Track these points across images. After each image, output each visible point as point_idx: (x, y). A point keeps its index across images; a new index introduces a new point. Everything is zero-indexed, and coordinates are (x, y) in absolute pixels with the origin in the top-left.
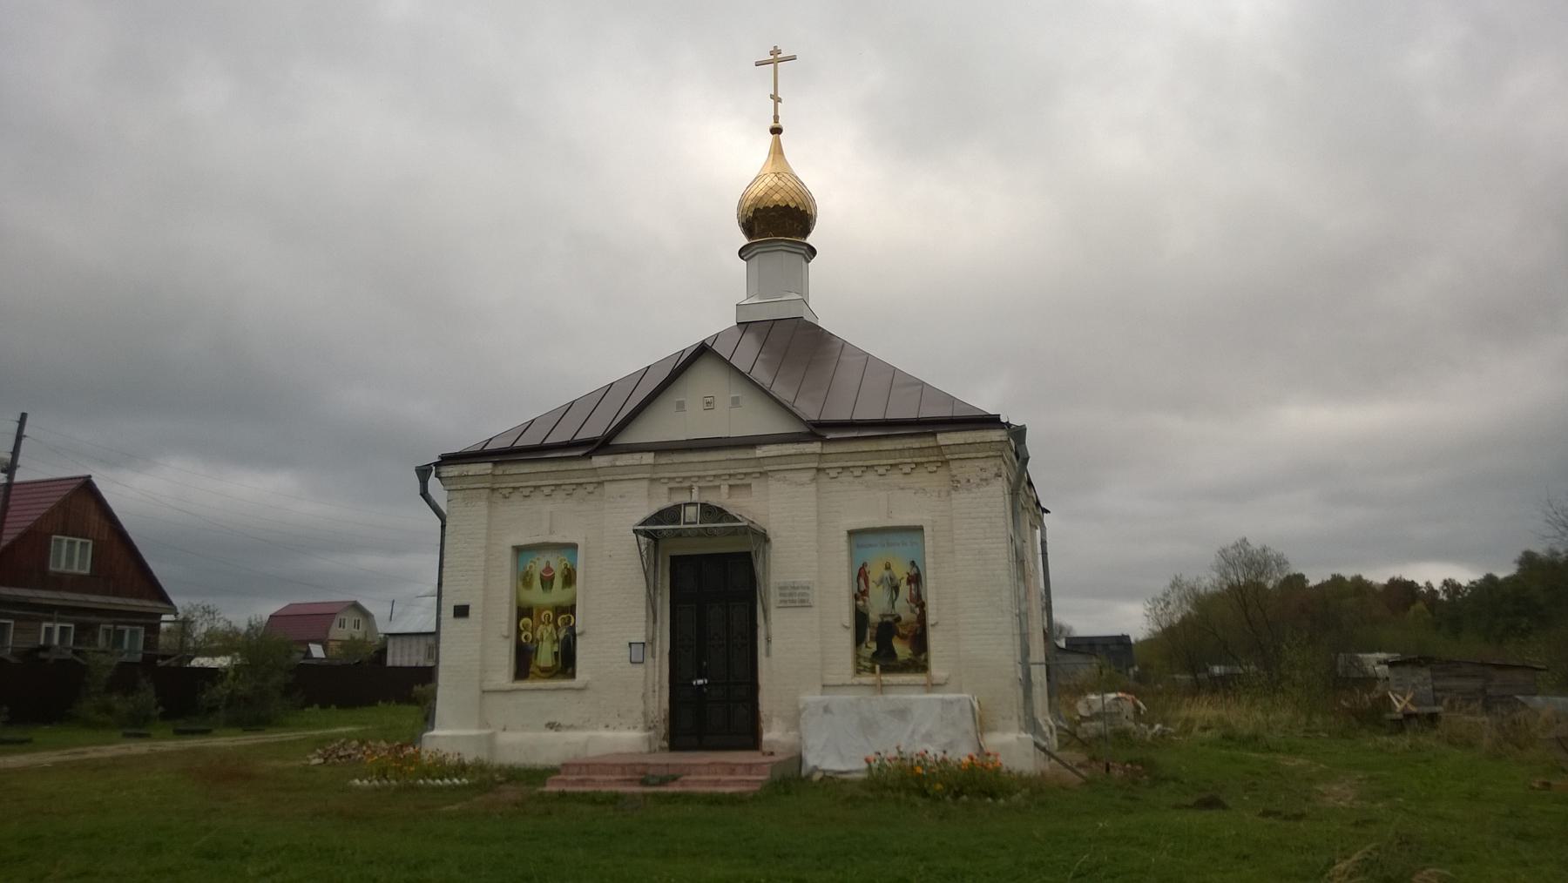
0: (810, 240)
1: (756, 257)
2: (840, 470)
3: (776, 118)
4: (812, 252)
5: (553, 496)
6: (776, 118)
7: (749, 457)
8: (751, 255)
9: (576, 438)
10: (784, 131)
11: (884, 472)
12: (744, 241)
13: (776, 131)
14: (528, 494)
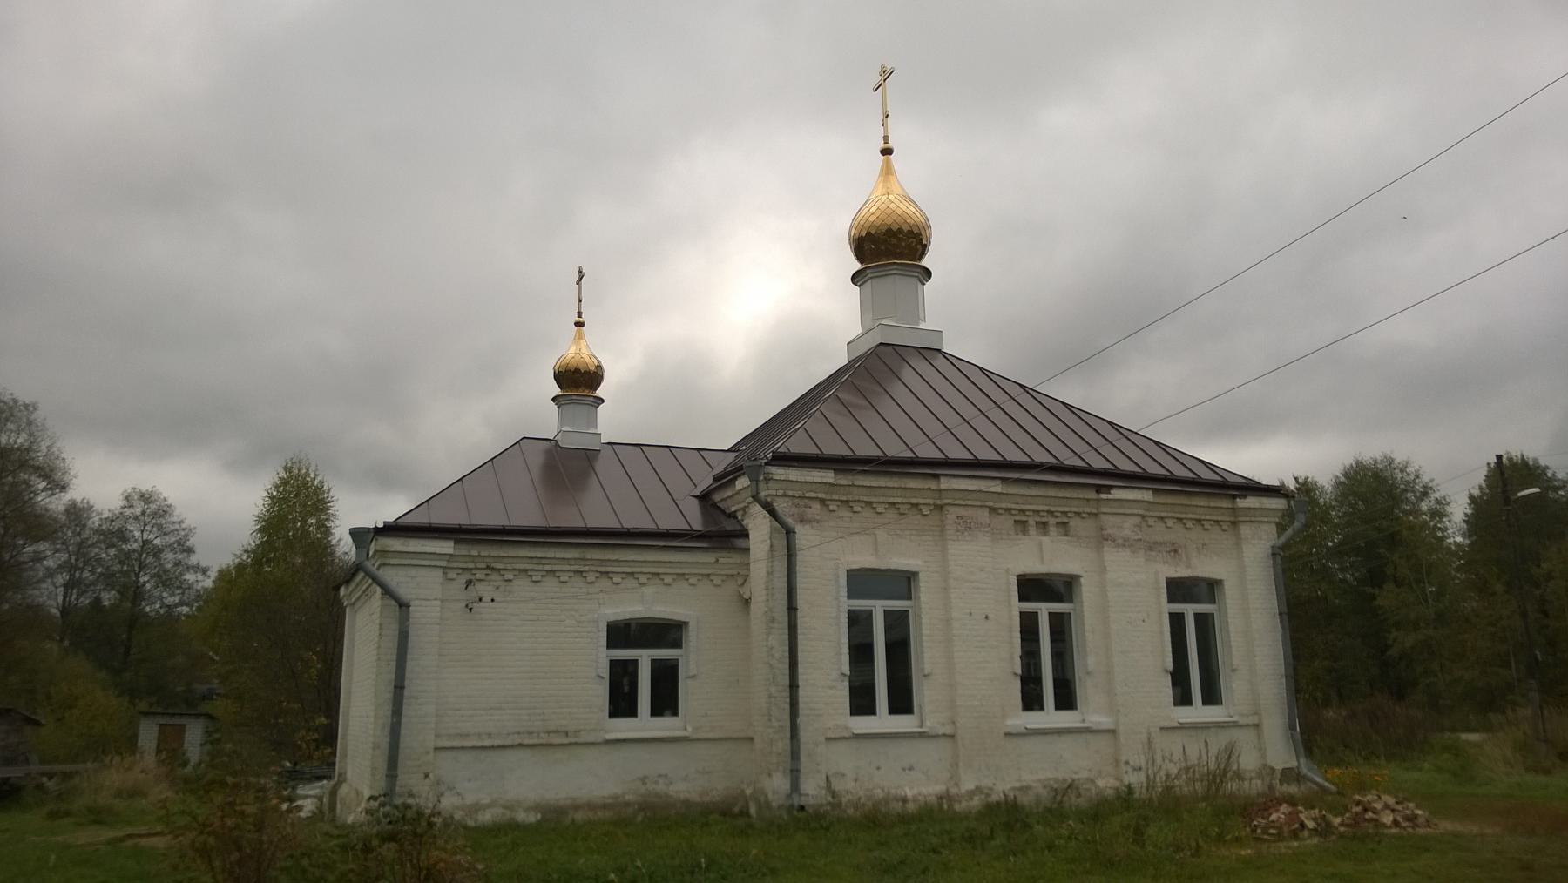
0: (925, 262)
1: (870, 282)
2: (460, 571)
3: (886, 139)
4: (927, 273)
5: (622, 586)
6: (886, 139)
7: (607, 558)
8: (876, 274)
10: (880, 155)
11: (539, 578)
12: (857, 266)
13: (887, 152)
14: (694, 583)
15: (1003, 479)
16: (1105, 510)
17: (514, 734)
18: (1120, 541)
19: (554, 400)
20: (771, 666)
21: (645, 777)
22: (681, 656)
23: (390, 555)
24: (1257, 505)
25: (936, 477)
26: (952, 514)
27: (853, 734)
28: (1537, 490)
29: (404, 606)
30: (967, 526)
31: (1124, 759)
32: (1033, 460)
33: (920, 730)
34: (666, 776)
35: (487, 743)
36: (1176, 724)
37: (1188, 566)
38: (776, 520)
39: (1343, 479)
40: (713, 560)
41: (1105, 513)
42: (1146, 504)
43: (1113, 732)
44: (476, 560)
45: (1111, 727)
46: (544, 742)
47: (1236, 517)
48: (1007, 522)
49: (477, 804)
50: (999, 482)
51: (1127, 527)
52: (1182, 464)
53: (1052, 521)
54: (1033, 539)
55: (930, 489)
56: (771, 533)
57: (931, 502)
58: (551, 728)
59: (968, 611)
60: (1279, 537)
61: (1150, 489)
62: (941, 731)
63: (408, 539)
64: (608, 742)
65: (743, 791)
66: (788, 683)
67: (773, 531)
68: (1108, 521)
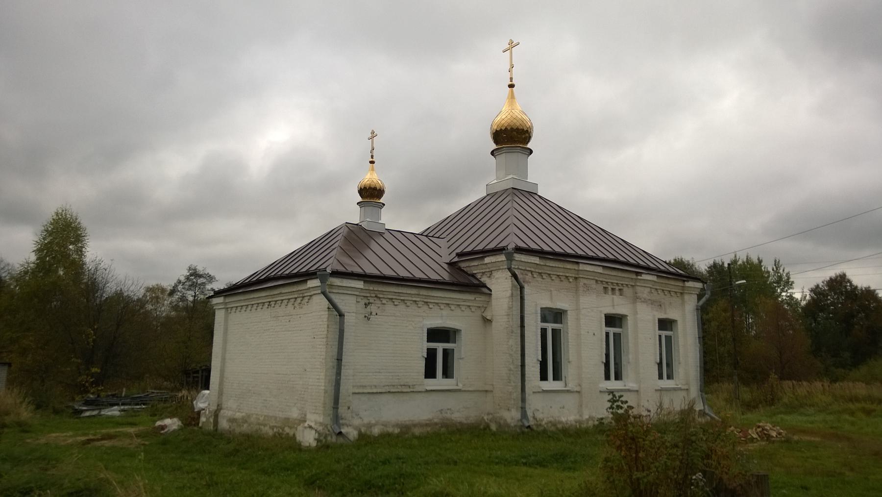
0: (529, 146)
3: (511, 79)
4: (531, 152)
5: (432, 310)
6: (511, 79)
7: (428, 295)
8: (500, 153)
9: (486, 248)
11: (398, 303)
13: (511, 86)
15: (604, 267)
16: (638, 284)
17: (386, 386)
18: (643, 300)
19: (358, 204)
20: (511, 355)
21: (442, 410)
22: (456, 347)
23: (334, 287)
24: (692, 286)
25: (578, 263)
26: (582, 282)
27: (543, 390)
28: (745, 281)
29: (341, 315)
30: (587, 288)
31: (642, 404)
32: (588, 255)
33: (565, 389)
34: (450, 409)
35: (375, 391)
36: (660, 388)
37: (665, 313)
38: (517, 282)
39: (864, 289)
40: (473, 299)
41: (638, 286)
42: (653, 282)
43: (637, 391)
44: (372, 292)
45: (637, 389)
46: (400, 390)
47: (683, 290)
48: (600, 287)
49: (369, 423)
50: (601, 268)
51: (644, 293)
52: (412, 242)
53: (617, 288)
54: (609, 297)
55: (575, 269)
56: (512, 287)
57: (574, 276)
58: (402, 384)
59: (587, 331)
60: (698, 302)
61: (655, 275)
62: (575, 390)
63: (343, 279)
64: (427, 391)
65: (483, 417)
66: (520, 364)
67: (513, 286)
68: (639, 289)
